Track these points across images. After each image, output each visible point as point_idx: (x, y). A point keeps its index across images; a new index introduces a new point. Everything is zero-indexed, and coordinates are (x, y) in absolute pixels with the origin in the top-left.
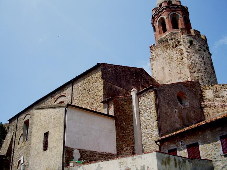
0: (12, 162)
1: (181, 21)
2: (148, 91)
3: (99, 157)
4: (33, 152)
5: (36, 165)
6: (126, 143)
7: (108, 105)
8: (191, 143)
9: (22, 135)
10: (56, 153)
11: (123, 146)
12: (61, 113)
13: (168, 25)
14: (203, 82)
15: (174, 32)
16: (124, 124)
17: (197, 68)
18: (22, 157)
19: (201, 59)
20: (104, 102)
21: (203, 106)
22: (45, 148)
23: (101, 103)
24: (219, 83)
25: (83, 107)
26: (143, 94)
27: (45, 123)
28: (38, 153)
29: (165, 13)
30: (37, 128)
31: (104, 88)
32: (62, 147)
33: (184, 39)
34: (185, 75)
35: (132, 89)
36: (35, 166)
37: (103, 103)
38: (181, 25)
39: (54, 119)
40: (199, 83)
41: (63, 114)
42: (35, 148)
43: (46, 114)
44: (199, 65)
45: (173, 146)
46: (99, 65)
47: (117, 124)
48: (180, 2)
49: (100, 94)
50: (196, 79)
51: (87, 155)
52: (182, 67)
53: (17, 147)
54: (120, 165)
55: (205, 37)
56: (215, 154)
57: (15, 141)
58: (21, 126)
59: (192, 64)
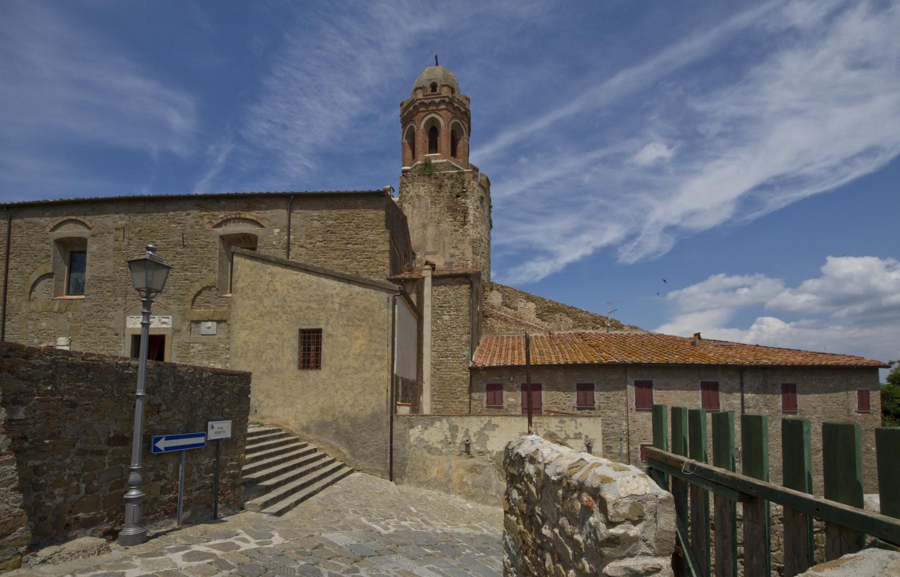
34: (463, 254)
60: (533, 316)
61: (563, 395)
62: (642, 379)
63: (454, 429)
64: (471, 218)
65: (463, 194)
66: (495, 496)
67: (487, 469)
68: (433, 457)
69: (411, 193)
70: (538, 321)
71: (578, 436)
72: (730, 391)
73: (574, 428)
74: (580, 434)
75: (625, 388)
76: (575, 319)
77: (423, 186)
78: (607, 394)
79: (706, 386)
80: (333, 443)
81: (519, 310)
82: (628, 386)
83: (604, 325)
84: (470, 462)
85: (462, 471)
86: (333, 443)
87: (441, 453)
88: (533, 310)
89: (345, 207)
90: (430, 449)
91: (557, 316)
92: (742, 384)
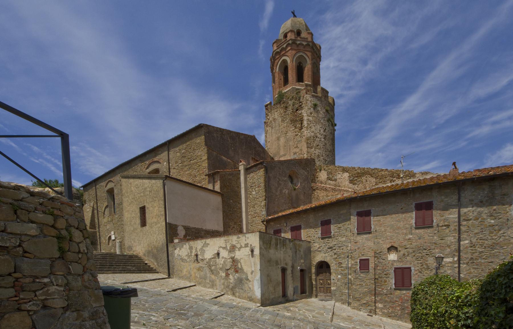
0: (100, 238)
1: (308, 70)
2: (258, 167)
3: (205, 234)
4: (128, 228)
5: (134, 242)
6: (232, 224)
7: (214, 179)
8: (295, 225)
9: (107, 207)
10: (157, 229)
11: (230, 224)
12: (159, 185)
13: (292, 75)
14: (319, 160)
15: (297, 87)
16: (231, 201)
17: (316, 142)
18: (112, 233)
19: (322, 131)
20: (209, 175)
21: (314, 188)
22: (143, 223)
23: (206, 175)
24: (337, 164)
25: (184, 179)
26: (252, 170)
27: (139, 195)
28: (135, 229)
29: (288, 54)
30: (129, 201)
31: (208, 159)
32: (164, 223)
33: (308, 99)
34: (301, 150)
35: (241, 162)
36: (133, 242)
37: (207, 177)
38: (308, 80)
39: (150, 192)
40: (314, 161)
41: (162, 187)
42: (130, 224)
43: (139, 185)
44: (319, 139)
45: (278, 227)
46: (199, 127)
47: (223, 201)
48: (312, 35)
49: (204, 165)
50: (313, 157)
51: (193, 232)
52: (300, 139)
53: (104, 221)
54: (226, 243)
55: (334, 100)
56: (314, 236)
57: (98, 214)
58: (103, 195)
59: (310, 137)
60: (347, 183)
61: (313, 230)
62: (363, 210)
63: (191, 248)
64: (305, 123)
65: (301, 107)
66: (209, 283)
67: (205, 268)
68: (184, 264)
69: (271, 119)
70: (351, 185)
71: (246, 245)
72: (446, 208)
73: (244, 241)
74: (248, 244)
75: (350, 219)
76: (376, 178)
77: (276, 111)
78: (339, 225)
79: (419, 207)
80: (152, 260)
81: (338, 180)
82: (352, 217)
83: (399, 177)
84: (198, 265)
85: (195, 270)
86: (152, 260)
87: (187, 262)
88: (347, 178)
89: (189, 140)
90: (183, 260)
91: (364, 178)
92: (459, 200)
